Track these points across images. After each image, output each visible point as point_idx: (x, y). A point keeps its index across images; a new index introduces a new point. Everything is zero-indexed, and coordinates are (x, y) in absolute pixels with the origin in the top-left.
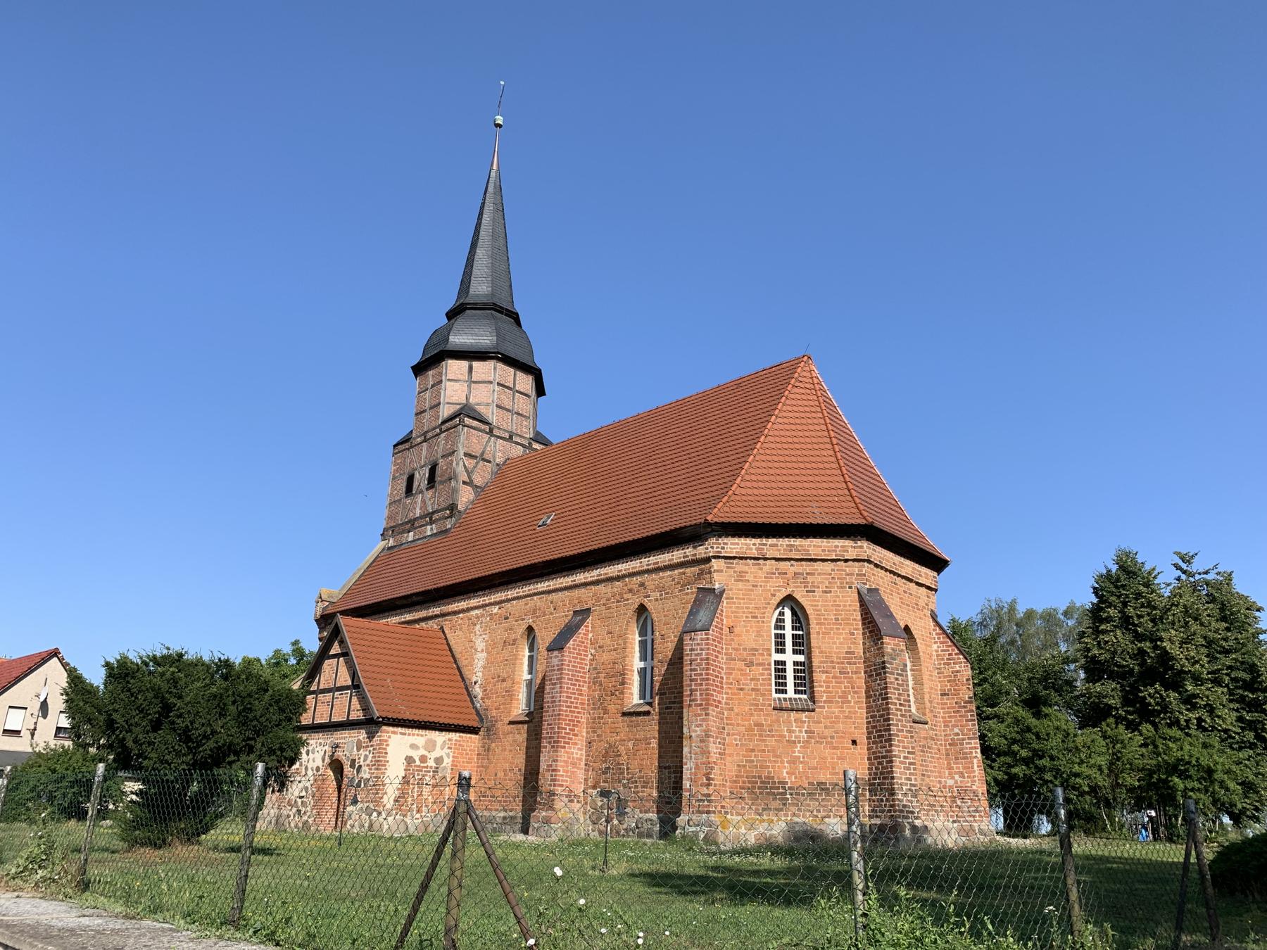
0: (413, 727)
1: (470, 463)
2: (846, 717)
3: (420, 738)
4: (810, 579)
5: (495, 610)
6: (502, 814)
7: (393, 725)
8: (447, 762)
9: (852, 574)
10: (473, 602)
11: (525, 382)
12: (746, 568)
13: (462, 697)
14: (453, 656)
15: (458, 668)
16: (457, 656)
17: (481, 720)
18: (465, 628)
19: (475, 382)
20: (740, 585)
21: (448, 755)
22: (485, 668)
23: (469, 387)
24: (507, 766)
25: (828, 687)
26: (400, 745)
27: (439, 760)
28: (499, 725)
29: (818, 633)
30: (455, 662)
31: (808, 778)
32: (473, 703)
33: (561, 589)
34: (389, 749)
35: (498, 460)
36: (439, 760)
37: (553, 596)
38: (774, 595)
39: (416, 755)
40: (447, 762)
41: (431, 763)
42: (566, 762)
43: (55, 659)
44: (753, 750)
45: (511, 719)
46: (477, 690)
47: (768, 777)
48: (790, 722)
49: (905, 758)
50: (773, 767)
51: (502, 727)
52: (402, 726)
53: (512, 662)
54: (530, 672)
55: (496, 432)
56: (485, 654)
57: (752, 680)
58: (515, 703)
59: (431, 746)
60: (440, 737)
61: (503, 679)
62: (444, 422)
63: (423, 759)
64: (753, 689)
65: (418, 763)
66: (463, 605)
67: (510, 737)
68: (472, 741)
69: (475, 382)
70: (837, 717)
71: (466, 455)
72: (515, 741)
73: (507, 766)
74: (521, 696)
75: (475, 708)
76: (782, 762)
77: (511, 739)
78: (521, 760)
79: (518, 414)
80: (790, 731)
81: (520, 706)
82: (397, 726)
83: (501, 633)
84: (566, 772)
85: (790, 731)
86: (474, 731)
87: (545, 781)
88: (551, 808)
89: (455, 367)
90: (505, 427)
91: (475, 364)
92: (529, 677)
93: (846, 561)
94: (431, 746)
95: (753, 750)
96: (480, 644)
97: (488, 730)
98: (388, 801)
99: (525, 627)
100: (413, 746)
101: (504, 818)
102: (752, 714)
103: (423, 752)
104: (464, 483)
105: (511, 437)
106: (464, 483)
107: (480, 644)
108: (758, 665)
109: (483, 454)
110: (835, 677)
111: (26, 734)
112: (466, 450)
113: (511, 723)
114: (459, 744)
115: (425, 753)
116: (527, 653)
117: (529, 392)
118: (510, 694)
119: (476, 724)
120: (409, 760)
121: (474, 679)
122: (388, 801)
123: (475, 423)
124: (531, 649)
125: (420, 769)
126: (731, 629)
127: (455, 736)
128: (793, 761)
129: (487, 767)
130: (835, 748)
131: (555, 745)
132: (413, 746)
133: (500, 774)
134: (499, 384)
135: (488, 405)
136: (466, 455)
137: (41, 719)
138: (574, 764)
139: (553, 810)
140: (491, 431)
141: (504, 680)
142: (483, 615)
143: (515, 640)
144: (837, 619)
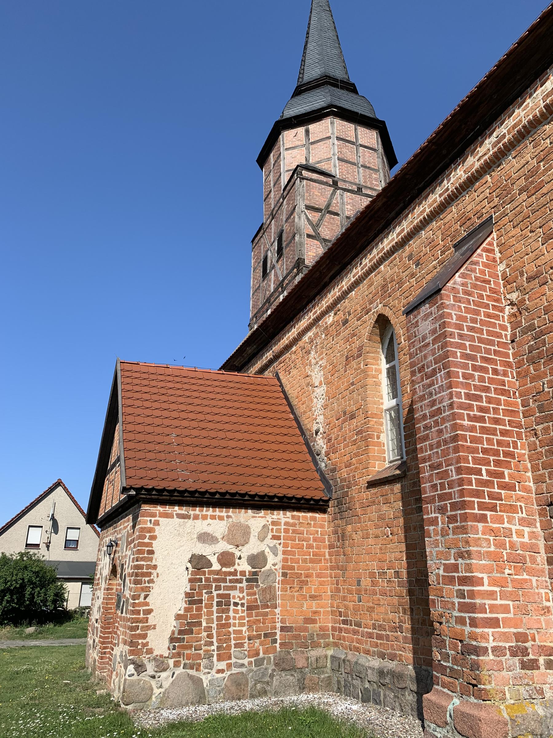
0: (202, 504)
1: (314, 216)
3: (216, 523)
5: (330, 319)
6: (376, 663)
7: (163, 503)
8: (274, 562)
10: (303, 323)
11: (370, 137)
13: (301, 457)
14: (290, 405)
15: (296, 420)
16: (294, 402)
17: (329, 488)
18: (299, 363)
19: (313, 143)
22: (325, 407)
23: (308, 149)
24: (374, 566)
26: (177, 539)
27: (257, 560)
28: (353, 492)
30: (293, 412)
32: (316, 463)
33: (425, 223)
34: (156, 545)
35: (347, 213)
36: (257, 560)
37: (414, 245)
40: (274, 562)
41: (244, 566)
42: (495, 557)
43: (60, 487)
45: (370, 478)
46: (320, 444)
51: (360, 495)
52: (181, 503)
53: (361, 385)
54: (395, 396)
55: (340, 184)
56: (324, 387)
58: (374, 450)
59: (239, 536)
60: (256, 520)
61: (352, 416)
62: (284, 190)
63: (226, 559)
65: (216, 566)
66: (293, 333)
67: (373, 513)
68: (317, 524)
69: (313, 143)
71: (308, 207)
72: (381, 518)
73: (374, 566)
74: (383, 438)
75: (319, 470)
77: (374, 515)
78: (397, 554)
79: (364, 166)
81: (385, 453)
82: (172, 503)
83: (340, 346)
84: (501, 583)
86: (318, 506)
87: (445, 602)
88: (473, 688)
89: (290, 137)
90: (351, 179)
91: (311, 127)
92: (394, 402)
96: (317, 376)
97: (340, 503)
98: (159, 642)
99: (371, 319)
100: (205, 538)
101: (381, 673)
103: (223, 546)
104: (309, 236)
105: (360, 190)
106: (309, 236)
107: (317, 376)
109: (328, 205)
111: (43, 547)
112: (308, 203)
113: (372, 484)
114: (293, 532)
116: (384, 366)
117: (375, 146)
118: (364, 437)
119: (318, 495)
120: (199, 563)
121: (315, 428)
122: (159, 642)
123: (315, 176)
124: (390, 357)
125: (221, 577)
127: (284, 517)
129: (344, 569)
131: (459, 516)
133: (366, 582)
134: (338, 139)
135: (329, 159)
136: (308, 207)
137: (53, 534)
138: (518, 562)
139: (483, 695)
140: (335, 184)
141: (353, 417)
142: (316, 335)
143: (360, 349)
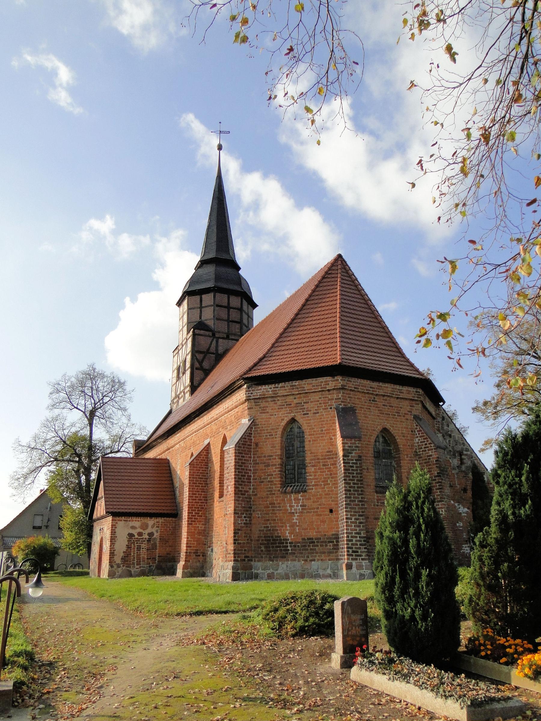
2: (326, 494)
4: (306, 406)
8: (156, 535)
9: (332, 399)
12: (267, 404)
20: (264, 416)
21: (157, 532)
25: (315, 476)
29: (310, 441)
31: (302, 536)
36: (151, 534)
38: (283, 420)
39: (135, 532)
40: (156, 535)
44: (268, 520)
47: (277, 537)
48: (291, 500)
49: (356, 519)
50: (280, 530)
57: (268, 475)
59: (145, 526)
60: (151, 522)
63: (140, 534)
64: (269, 481)
65: (136, 536)
70: (320, 495)
76: (286, 527)
80: (291, 506)
85: (291, 506)
93: (329, 390)
94: (145, 526)
95: (268, 520)
100: (133, 528)
102: (268, 498)
108: (273, 465)
110: (319, 469)
115: (141, 531)
120: (131, 535)
125: (138, 540)
126: (257, 444)
128: (293, 525)
130: (318, 515)
132: (133, 528)
140: (214, 335)
144: (322, 431)
